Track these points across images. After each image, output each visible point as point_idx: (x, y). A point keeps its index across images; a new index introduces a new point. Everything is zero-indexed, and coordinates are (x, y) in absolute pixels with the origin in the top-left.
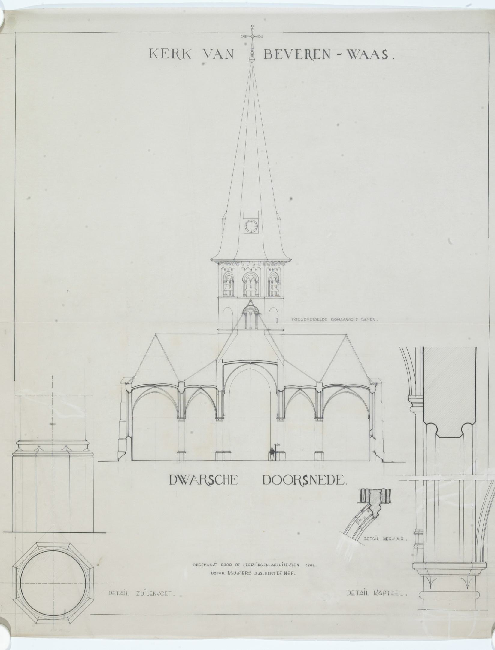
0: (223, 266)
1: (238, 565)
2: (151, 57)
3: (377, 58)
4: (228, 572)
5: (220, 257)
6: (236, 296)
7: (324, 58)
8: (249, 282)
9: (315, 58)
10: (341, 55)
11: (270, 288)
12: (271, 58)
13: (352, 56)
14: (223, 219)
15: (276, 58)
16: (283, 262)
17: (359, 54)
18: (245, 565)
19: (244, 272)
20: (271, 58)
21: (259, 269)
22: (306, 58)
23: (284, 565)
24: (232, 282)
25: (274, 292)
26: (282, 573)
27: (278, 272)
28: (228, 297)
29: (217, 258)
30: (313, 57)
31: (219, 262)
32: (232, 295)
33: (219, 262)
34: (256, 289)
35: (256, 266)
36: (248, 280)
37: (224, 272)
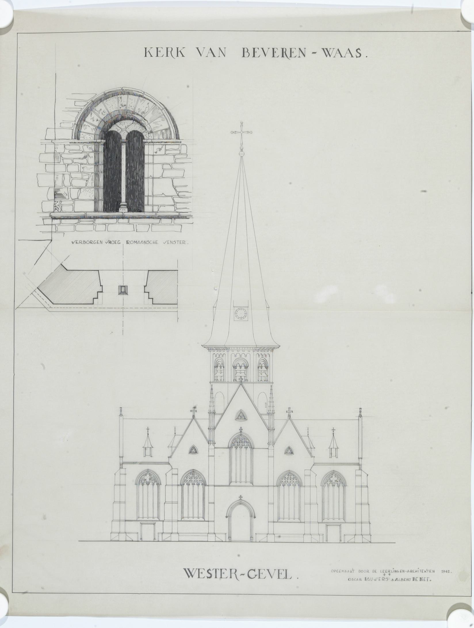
0: (214, 352)
1: (375, 571)
2: (146, 56)
3: (351, 56)
4: (365, 578)
5: (210, 343)
6: (227, 381)
7: (299, 57)
8: (239, 367)
9: (291, 56)
10: (312, 52)
11: (260, 373)
12: (248, 57)
13: (327, 55)
14: (213, 307)
15: (254, 56)
16: (272, 349)
17: (333, 53)
18: (382, 571)
19: (234, 358)
20: (248, 57)
21: (248, 355)
22: (283, 56)
23: (419, 571)
24: (222, 367)
25: (263, 377)
26: (418, 579)
27: (267, 358)
28: (218, 382)
29: (207, 344)
30: (289, 55)
31: (210, 349)
32: (222, 380)
33: (210, 349)
34: (246, 374)
35: (246, 352)
36: (238, 365)
37: (215, 358)
